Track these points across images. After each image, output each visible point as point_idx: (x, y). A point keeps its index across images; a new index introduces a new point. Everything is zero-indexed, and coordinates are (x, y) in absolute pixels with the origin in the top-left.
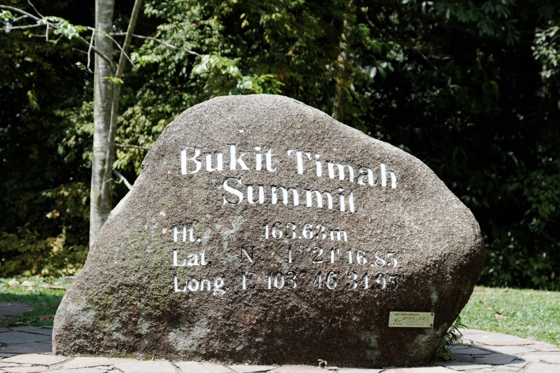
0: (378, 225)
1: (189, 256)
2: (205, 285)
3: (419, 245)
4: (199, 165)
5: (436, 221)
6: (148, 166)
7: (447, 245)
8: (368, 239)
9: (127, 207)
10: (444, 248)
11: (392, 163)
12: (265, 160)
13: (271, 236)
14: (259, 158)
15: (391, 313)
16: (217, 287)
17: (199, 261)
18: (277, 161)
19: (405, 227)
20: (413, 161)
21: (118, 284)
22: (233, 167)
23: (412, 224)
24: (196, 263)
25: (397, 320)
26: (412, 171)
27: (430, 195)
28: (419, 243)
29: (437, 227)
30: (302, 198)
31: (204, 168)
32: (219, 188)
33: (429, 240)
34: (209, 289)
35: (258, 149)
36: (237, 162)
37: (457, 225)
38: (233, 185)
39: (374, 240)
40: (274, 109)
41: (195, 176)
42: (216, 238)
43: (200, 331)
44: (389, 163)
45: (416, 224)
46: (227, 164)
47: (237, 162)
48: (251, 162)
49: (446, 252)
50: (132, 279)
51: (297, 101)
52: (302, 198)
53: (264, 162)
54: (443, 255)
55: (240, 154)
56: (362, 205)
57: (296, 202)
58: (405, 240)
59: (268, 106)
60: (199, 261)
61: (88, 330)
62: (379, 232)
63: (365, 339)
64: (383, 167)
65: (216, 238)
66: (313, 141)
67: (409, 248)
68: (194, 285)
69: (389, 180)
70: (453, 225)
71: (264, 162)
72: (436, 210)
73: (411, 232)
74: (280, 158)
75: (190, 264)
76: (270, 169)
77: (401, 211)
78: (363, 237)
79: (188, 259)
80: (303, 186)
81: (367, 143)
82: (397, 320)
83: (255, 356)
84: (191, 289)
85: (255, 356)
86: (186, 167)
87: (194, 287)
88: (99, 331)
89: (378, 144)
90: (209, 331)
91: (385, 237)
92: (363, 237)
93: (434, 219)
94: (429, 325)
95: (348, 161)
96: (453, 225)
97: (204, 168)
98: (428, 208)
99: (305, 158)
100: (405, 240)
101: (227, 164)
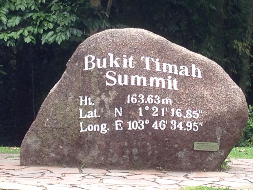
0: (189, 96)
1: (88, 113)
2: (97, 128)
3: (211, 107)
4: (94, 65)
5: (221, 95)
6: (69, 66)
7: (226, 107)
8: (183, 104)
9: (57, 88)
10: (225, 108)
11: (199, 64)
12: (129, 62)
13: (130, 102)
14: (125, 61)
15: (195, 142)
16: (102, 129)
17: (94, 115)
18: (135, 63)
19: (204, 97)
20: (212, 63)
21: (52, 128)
22: (111, 66)
23: (208, 96)
24: (92, 116)
25: (198, 146)
26: (210, 68)
27: (220, 81)
28: (211, 106)
29: (222, 97)
30: (148, 82)
31: (96, 66)
32: (104, 77)
33: (217, 104)
34: (98, 130)
35: (125, 56)
36: (114, 62)
37: (232, 97)
38: (110, 74)
39: (187, 104)
40: (135, 36)
41: (92, 70)
42: (102, 104)
43: (95, 153)
44: (197, 64)
45: (210, 96)
46: (108, 64)
47: (114, 62)
48: (120, 62)
49: (225, 111)
50: (60, 125)
51: (149, 32)
52: (148, 82)
53: (128, 63)
54: (224, 112)
55: (115, 59)
56: (181, 86)
57: (145, 84)
58: (203, 104)
59: (132, 34)
60: (94, 115)
61: (37, 152)
62: (189, 100)
63: (181, 157)
64: (193, 66)
65: (102, 104)
66: (162, 54)
67: (205, 108)
68: (91, 128)
69: (197, 74)
70: (230, 97)
71: (128, 63)
72: (222, 89)
73: (207, 100)
74: (137, 61)
75: (89, 117)
76: (131, 67)
77: (202, 89)
78: (181, 103)
79: (88, 114)
80: (148, 75)
81: (186, 54)
82: (198, 146)
83: (123, 165)
84: (90, 130)
85: (123, 165)
86: (112, 80)
87: (91, 128)
88: (43, 153)
89: (192, 54)
90: (99, 152)
91: (193, 102)
92: (181, 103)
93: (220, 94)
94: (217, 149)
95: (174, 63)
96: (230, 97)
97: (96, 66)
98: (217, 88)
99: (151, 61)
100: (203, 104)
101: (108, 64)
